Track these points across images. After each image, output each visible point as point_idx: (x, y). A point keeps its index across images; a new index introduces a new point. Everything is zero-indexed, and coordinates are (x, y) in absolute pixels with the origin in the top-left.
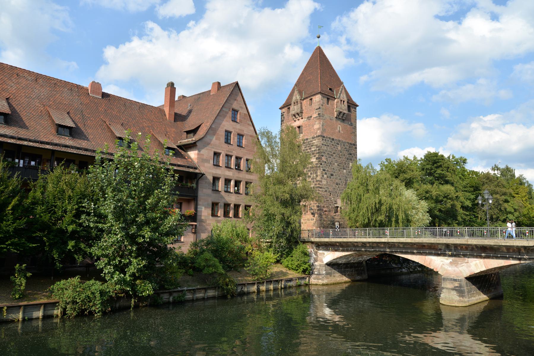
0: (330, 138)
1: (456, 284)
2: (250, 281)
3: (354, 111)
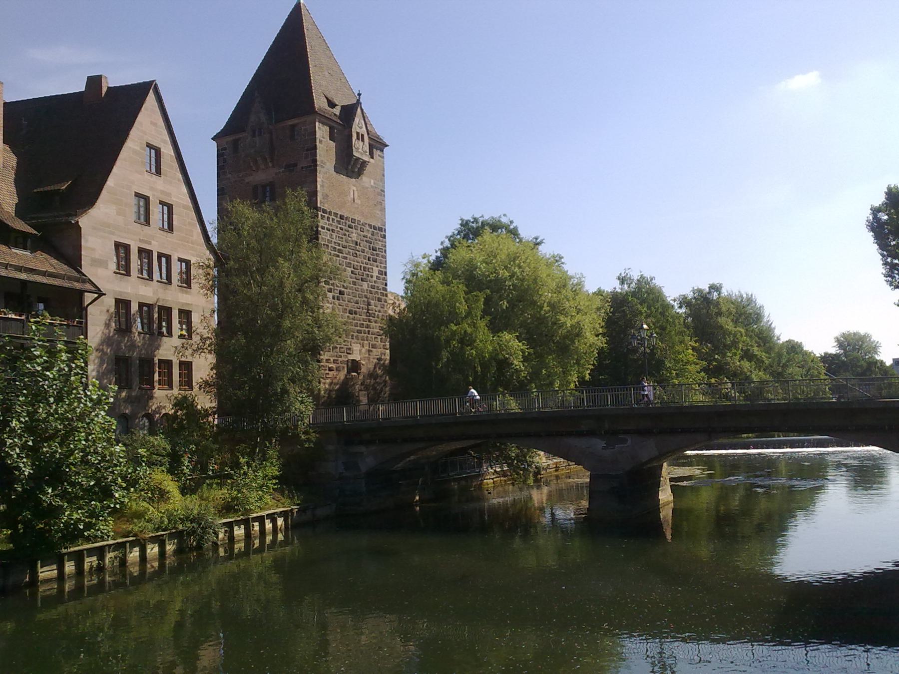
3: (379, 155)
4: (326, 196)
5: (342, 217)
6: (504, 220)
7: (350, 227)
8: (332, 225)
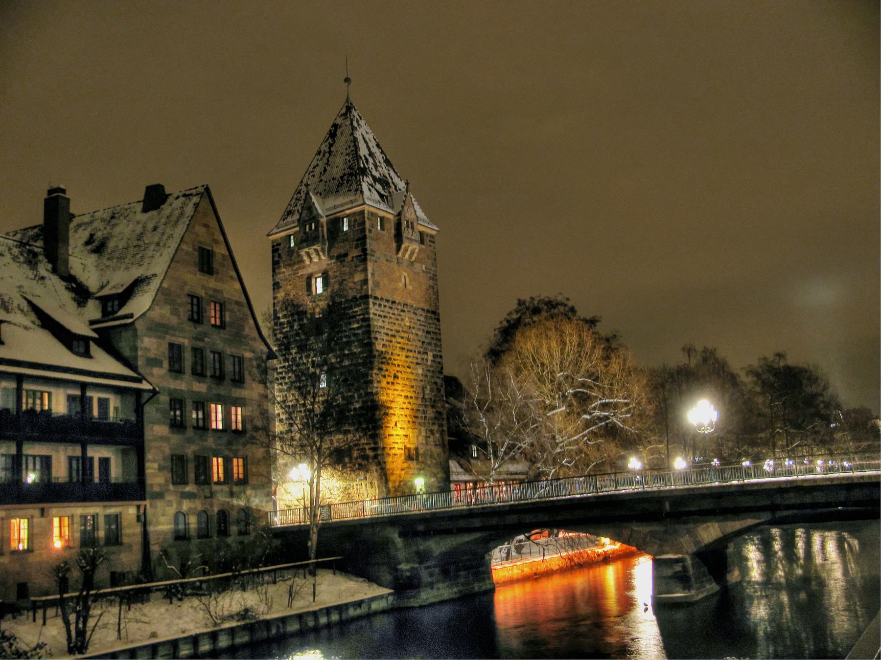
0: (388, 301)
1: (678, 568)
2: (47, 594)
3: (430, 241)
4: (377, 284)
5: (394, 302)
6: (560, 298)
7: (403, 311)
8: (383, 311)
